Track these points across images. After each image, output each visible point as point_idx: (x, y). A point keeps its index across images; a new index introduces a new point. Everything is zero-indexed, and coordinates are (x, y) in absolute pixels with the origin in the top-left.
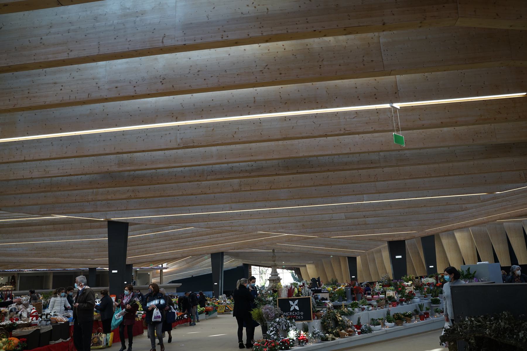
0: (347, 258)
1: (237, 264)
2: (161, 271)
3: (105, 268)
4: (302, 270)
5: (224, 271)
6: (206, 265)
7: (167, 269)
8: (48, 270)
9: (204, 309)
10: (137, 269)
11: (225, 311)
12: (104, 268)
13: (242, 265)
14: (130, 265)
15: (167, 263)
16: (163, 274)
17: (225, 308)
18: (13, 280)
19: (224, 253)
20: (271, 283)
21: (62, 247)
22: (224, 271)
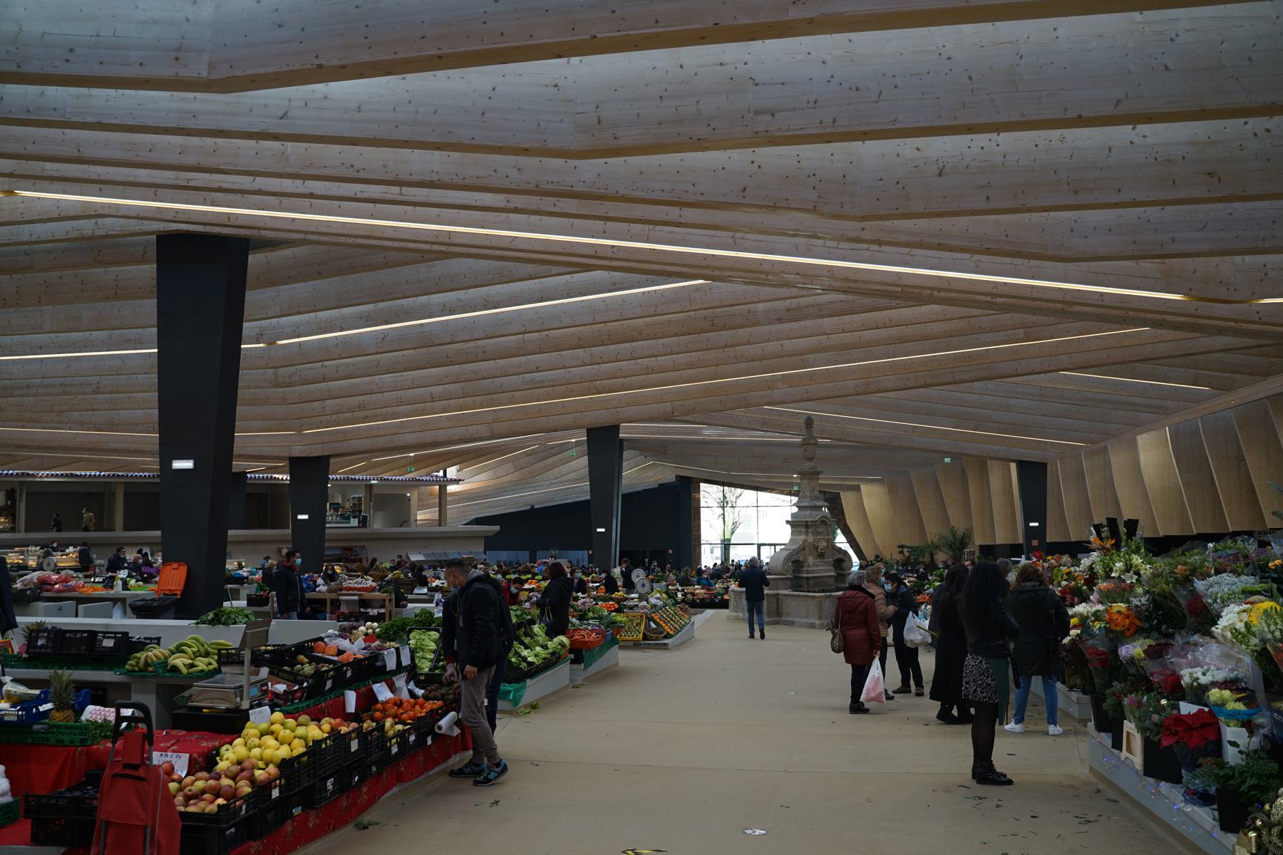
0: (1013, 466)
1: (659, 477)
2: (443, 488)
3: (277, 476)
4: (847, 499)
6: (572, 476)
7: (458, 484)
8: (150, 476)
9: (562, 645)
10: (373, 482)
11: (645, 638)
12: (274, 476)
13: (674, 480)
14: (318, 458)
15: (457, 467)
16: (449, 499)
17: (647, 626)
19: (625, 444)
20: (800, 533)
21: (65, 385)
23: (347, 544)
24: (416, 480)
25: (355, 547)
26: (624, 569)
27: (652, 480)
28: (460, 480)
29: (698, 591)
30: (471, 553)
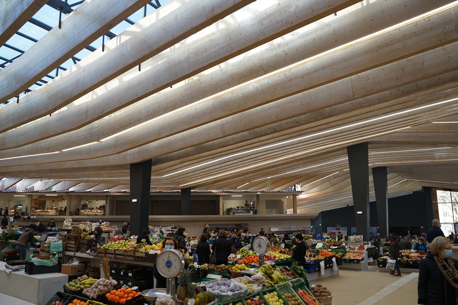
1: (412, 188)
5: (389, 199)
10: (258, 193)
13: (421, 189)
18: (348, 261)
22: (389, 199)
23: (239, 223)
24: (264, 192)
25: (242, 224)
26: (37, 232)
27: (408, 189)
28: (302, 192)
29: (412, 255)
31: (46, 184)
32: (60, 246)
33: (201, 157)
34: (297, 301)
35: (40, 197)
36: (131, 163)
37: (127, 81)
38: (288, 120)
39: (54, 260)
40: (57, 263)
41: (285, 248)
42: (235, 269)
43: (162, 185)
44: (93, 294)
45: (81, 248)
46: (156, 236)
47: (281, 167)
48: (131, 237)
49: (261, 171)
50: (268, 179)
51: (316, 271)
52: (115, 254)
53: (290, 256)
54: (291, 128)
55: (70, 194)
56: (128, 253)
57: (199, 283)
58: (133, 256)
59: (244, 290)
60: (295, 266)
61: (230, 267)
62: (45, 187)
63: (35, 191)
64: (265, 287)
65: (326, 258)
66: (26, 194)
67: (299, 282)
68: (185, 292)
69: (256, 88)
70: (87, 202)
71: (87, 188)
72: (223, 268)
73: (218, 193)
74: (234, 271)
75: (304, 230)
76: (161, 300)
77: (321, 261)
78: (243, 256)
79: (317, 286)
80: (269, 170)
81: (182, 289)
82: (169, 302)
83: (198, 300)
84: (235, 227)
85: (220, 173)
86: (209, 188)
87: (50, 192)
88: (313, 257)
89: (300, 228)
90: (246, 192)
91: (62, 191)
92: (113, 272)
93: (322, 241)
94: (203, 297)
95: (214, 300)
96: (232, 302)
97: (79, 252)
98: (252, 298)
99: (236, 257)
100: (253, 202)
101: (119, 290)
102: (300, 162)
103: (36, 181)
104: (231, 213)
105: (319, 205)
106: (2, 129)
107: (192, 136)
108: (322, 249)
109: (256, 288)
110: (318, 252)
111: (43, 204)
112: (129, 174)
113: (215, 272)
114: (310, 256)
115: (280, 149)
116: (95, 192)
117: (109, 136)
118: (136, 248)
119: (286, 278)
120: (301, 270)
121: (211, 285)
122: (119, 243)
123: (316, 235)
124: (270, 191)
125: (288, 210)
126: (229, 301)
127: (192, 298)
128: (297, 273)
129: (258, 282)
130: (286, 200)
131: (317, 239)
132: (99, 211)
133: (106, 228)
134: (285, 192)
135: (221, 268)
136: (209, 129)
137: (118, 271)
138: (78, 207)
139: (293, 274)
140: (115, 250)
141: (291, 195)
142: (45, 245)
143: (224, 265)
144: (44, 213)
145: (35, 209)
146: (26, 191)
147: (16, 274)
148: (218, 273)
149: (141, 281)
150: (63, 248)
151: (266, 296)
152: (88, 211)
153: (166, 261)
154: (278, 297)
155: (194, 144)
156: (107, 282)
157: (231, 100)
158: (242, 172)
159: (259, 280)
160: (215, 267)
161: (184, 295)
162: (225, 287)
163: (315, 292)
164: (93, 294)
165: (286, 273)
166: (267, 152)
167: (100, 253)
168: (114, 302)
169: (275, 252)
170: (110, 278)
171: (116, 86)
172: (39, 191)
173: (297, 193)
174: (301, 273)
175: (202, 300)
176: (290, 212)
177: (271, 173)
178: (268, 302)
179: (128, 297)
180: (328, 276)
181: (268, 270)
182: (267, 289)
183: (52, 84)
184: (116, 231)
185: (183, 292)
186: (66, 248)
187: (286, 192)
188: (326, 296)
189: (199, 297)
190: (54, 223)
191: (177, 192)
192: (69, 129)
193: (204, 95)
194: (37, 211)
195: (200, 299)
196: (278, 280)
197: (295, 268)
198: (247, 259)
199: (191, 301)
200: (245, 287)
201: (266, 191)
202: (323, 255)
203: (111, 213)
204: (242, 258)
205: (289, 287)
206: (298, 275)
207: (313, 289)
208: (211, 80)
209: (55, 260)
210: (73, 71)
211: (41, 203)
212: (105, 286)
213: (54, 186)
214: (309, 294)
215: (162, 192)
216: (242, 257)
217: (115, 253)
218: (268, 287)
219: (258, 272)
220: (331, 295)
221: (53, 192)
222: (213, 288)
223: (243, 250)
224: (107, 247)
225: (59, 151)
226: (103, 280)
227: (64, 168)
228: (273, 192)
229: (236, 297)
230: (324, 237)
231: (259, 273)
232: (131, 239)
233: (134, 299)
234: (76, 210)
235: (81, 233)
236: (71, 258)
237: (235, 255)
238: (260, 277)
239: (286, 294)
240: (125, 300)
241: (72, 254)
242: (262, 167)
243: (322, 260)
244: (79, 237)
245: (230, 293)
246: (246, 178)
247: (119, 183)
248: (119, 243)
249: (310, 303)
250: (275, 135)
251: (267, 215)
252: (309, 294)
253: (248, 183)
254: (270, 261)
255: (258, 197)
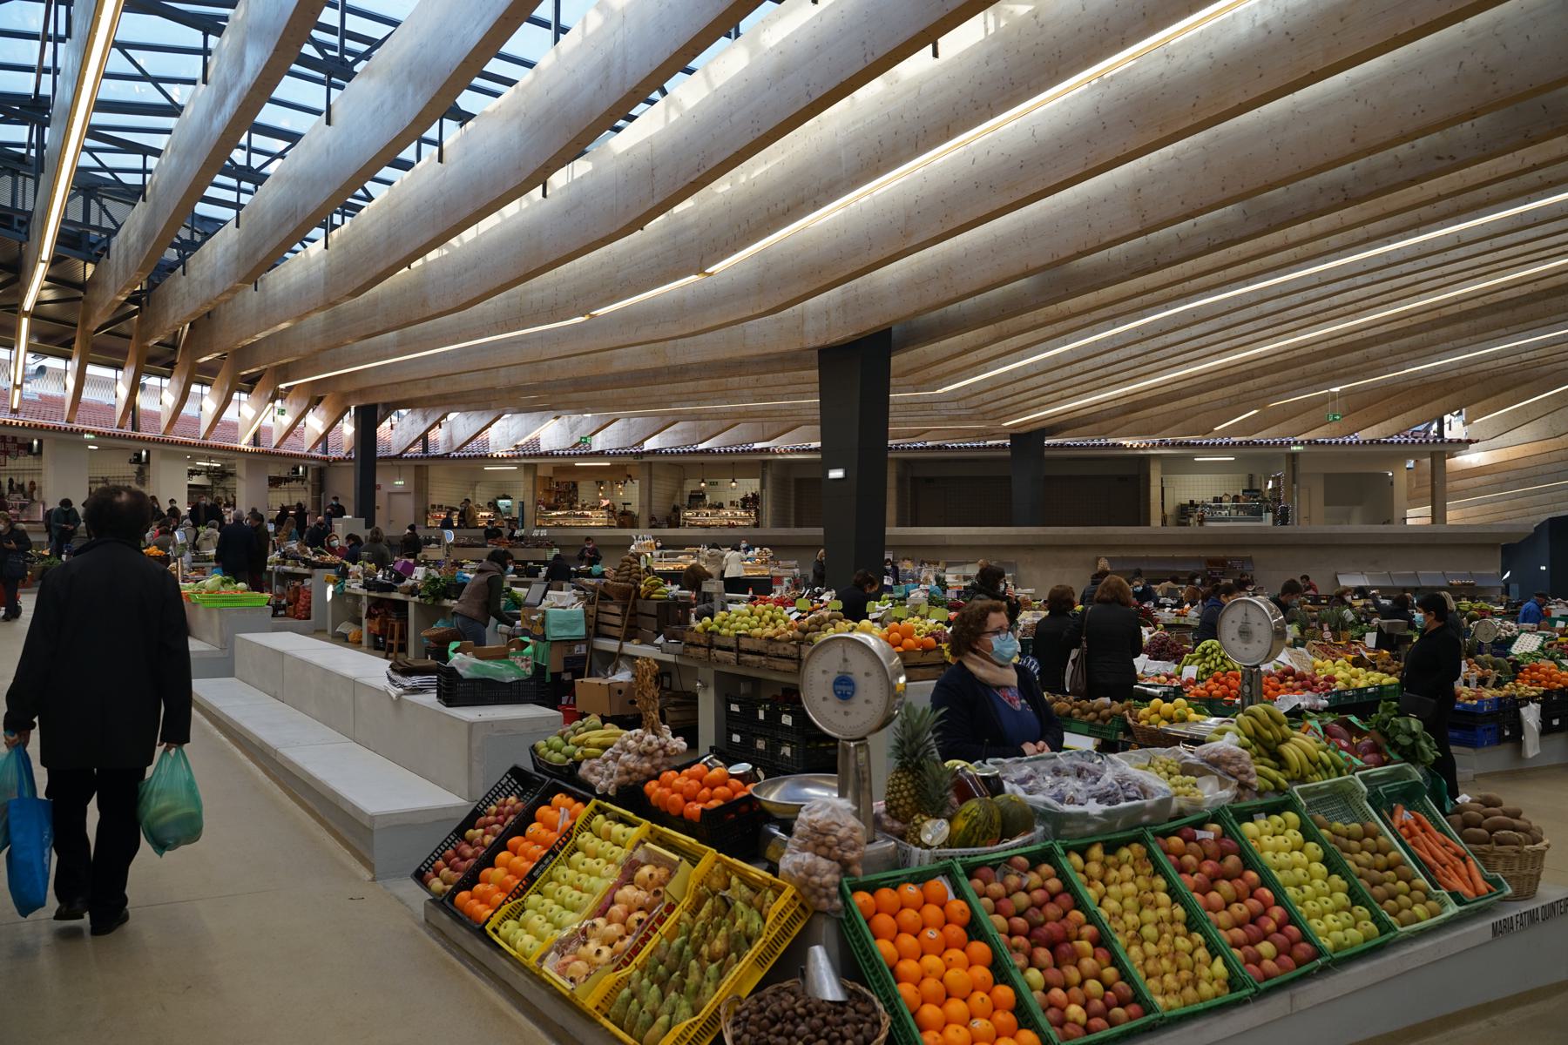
10: (1294, 448)
24: (1316, 443)
25: (1231, 559)
28: (1470, 442)
30: (1471, 576)
31: (572, 429)
32: (576, 621)
33: (1067, 313)
34: (1386, 855)
35: (559, 469)
36: (818, 344)
37: (776, 45)
38: (1403, 150)
39: (519, 663)
40: (530, 673)
41: (1379, 645)
42: (1148, 715)
43: (945, 422)
44: (607, 779)
45: (640, 629)
46: (921, 595)
47: (1385, 347)
48: (821, 598)
49: (1304, 364)
50: (1334, 396)
51: (1501, 740)
52: (740, 651)
53: (1394, 679)
54: (1413, 182)
55: (646, 459)
56: (777, 649)
57: (979, 762)
58: (793, 659)
59: (1157, 798)
60: (1385, 716)
61: (1129, 707)
62: (572, 438)
63: (542, 450)
64: (1248, 790)
65: (1547, 694)
66: (516, 461)
67: (1397, 781)
68: (913, 792)
69: (1265, 25)
70: (703, 485)
71: (698, 440)
72: (1105, 712)
73: (1144, 448)
74: (1143, 723)
75: (1473, 584)
76: (811, 817)
77: (1527, 705)
78: (1208, 671)
79: (1480, 802)
80: (1336, 359)
81: (904, 781)
82: (841, 827)
83: (961, 824)
84: (1204, 568)
85: (1145, 374)
86: (1109, 432)
87: (586, 454)
88: (1494, 686)
89: (1457, 579)
90: (1247, 443)
91: (622, 449)
92: (735, 708)
93: (1539, 629)
94: (982, 816)
95: (1029, 828)
96: (1101, 842)
97: (635, 641)
98: (1190, 829)
99: (1180, 674)
100: (1273, 479)
101: (686, 771)
102: (1463, 326)
103: (542, 421)
104: (1191, 521)
105: (1540, 492)
106: (407, 253)
107: (1025, 236)
108: (1538, 657)
109: (1211, 793)
110: (1516, 667)
111: (570, 491)
112: (817, 386)
113: (1074, 725)
114: (1482, 681)
115: (1376, 276)
116: (725, 451)
117: (736, 251)
118: (805, 632)
119: (1341, 762)
120: (1412, 735)
121: (1026, 770)
122: (752, 615)
123: (1521, 604)
124: (1340, 441)
125: (1410, 512)
126: (1092, 835)
127: (938, 818)
128: (1395, 746)
129: (1219, 772)
130: (1403, 474)
131: (1520, 619)
132: (740, 513)
133: (763, 567)
134: (1399, 442)
135: (1097, 711)
136: (1089, 205)
137: (750, 706)
138: (677, 502)
139: (1375, 748)
140: (740, 635)
141: (1423, 454)
142: (534, 618)
143: (1107, 700)
144: (572, 522)
145: (547, 509)
146: (516, 453)
147: (413, 704)
148: (1085, 728)
149: (823, 745)
150: (588, 627)
151: (1249, 828)
152: (707, 515)
153: (833, 676)
154: (1300, 835)
155: (1032, 265)
156: (650, 744)
157: (1165, 86)
158: (1232, 371)
159: (1224, 762)
160: (1075, 707)
161: (911, 804)
162: (1079, 784)
163: (1467, 824)
164: (607, 779)
165: (1344, 743)
166: (1323, 290)
167: (692, 644)
168: (668, 812)
169: (1334, 662)
170: (660, 729)
171: (742, 67)
172: (555, 453)
173: (1449, 448)
174: (1413, 744)
175: (977, 825)
176: (1417, 517)
177: (1342, 371)
178: (1257, 851)
179: (712, 799)
180: (1555, 763)
181: (1268, 728)
182: (1258, 801)
183: (530, 83)
184: (794, 578)
185: (905, 793)
186: (596, 627)
187: (1406, 442)
188: (1516, 844)
189: (967, 815)
190: (594, 551)
191: (997, 446)
192: (604, 234)
193: (1057, 73)
194: (554, 514)
195: (970, 823)
196: (1308, 767)
197: (1386, 723)
198: (1222, 684)
199: (933, 827)
200: (1160, 784)
201: (1327, 441)
202: (1539, 682)
203: (781, 521)
204: (1204, 677)
205: (1355, 796)
206: (1400, 754)
207: (1459, 809)
208: (1081, 10)
209: (523, 664)
210: (590, 29)
211: (563, 488)
212: (642, 754)
213: (599, 434)
214: (1442, 830)
215: (947, 447)
216: (1202, 673)
217: (738, 647)
218: (1260, 793)
219: (1222, 733)
220: (1541, 840)
221: (597, 453)
222: (1031, 783)
223: (1209, 651)
224: (715, 627)
225: (583, 316)
226: (636, 735)
227: (612, 371)
228: (1351, 442)
229: (1118, 825)
230: (1555, 614)
231: (1228, 736)
232: (822, 601)
233: (731, 805)
234: (670, 511)
235: (639, 579)
236: (611, 661)
237: (1176, 666)
238: (1229, 751)
239: (1338, 825)
240: (698, 807)
241: (611, 645)
242: (1309, 350)
243: (1533, 699)
244: (633, 592)
245: (1094, 808)
246: (1245, 392)
247: (797, 418)
248: (752, 615)
249: (1444, 866)
250: (1349, 214)
251: (1327, 529)
252: (1442, 830)
253: (1255, 412)
254: (1308, 693)
255: (1294, 461)
